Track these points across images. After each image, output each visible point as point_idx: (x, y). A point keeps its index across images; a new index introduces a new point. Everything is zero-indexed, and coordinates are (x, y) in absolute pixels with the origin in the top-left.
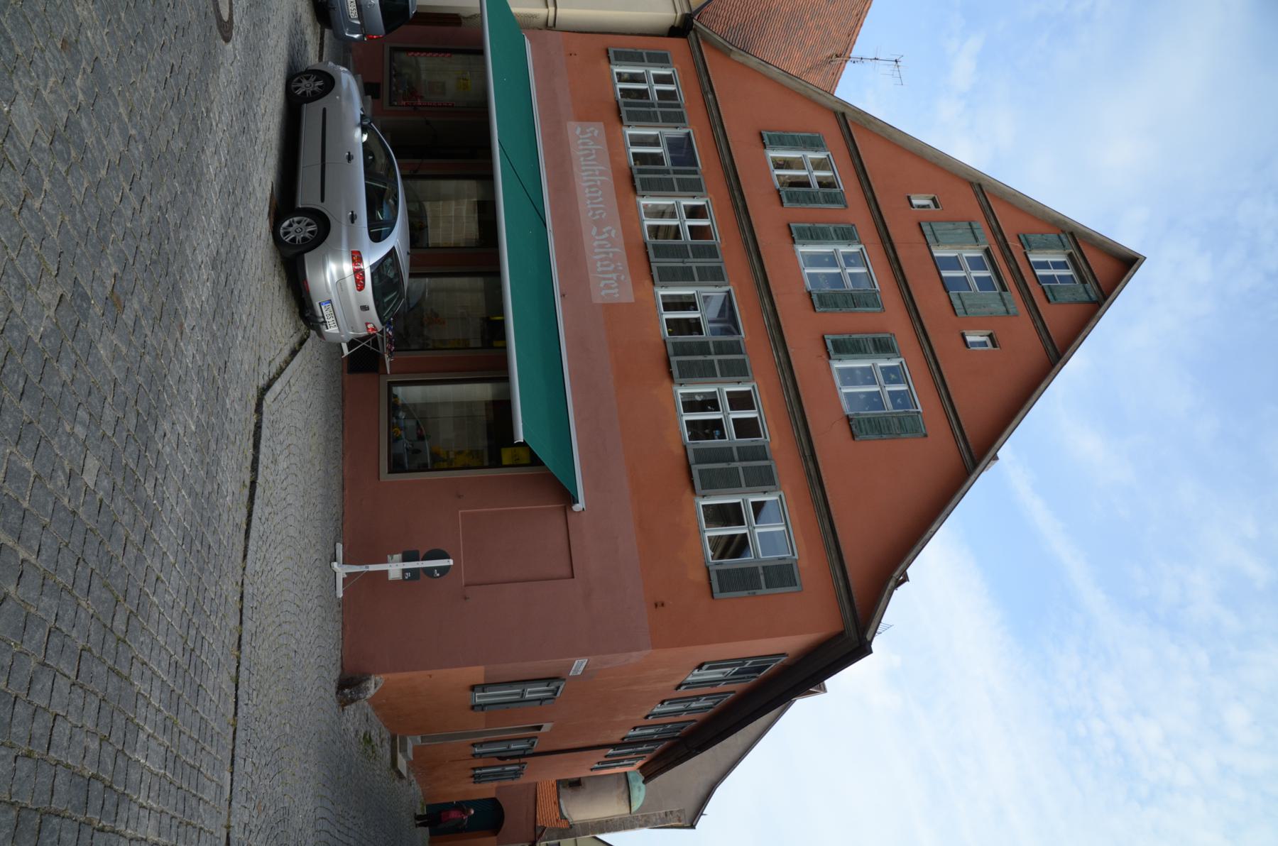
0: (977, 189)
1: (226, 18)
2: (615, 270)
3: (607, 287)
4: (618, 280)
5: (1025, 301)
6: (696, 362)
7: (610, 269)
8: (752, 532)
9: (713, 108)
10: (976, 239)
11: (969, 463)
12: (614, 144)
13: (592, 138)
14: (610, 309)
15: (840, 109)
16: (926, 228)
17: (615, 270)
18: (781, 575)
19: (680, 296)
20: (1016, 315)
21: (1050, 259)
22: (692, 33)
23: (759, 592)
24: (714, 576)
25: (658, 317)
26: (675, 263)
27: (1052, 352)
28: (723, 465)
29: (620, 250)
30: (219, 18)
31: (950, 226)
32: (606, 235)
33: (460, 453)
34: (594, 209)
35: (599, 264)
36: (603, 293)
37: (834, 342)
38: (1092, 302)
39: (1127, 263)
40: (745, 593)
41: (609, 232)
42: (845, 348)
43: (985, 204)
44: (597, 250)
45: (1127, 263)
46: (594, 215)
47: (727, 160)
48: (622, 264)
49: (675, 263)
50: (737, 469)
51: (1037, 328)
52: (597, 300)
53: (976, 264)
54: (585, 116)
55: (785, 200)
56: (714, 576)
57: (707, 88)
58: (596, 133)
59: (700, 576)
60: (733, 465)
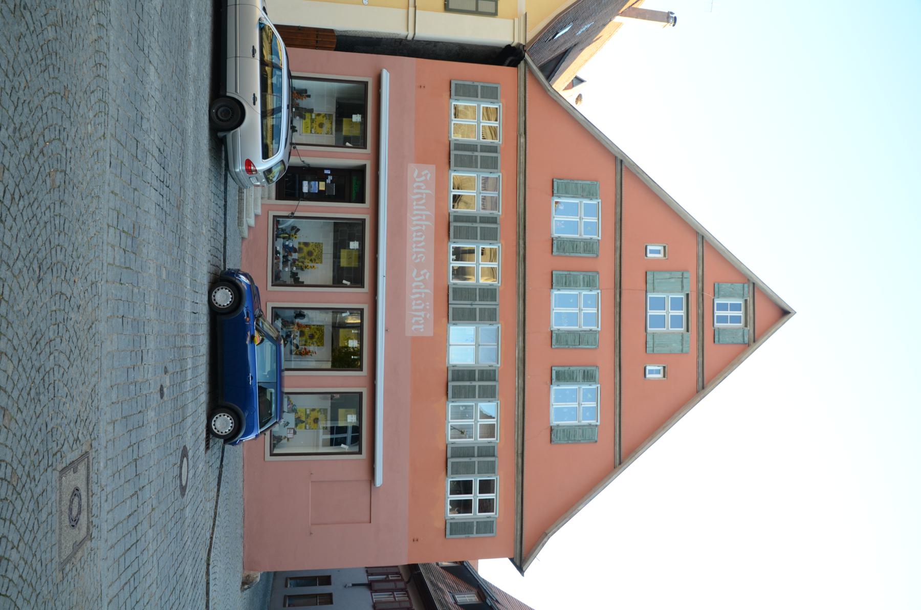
0: (700, 240)
1: (184, 483)
2: (424, 309)
3: (417, 323)
4: (425, 318)
5: (698, 340)
6: (465, 386)
7: (421, 307)
8: (477, 267)
9: (522, 153)
10: (683, 287)
11: (618, 461)
12: (440, 185)
13: (423, 281)
14: (415, 339)
15: (620, 157)
16: (649, 277)
17: (424, 309)
18: (489, 293)
19: (465, 243)
20: (687, 353)
21: (729, 325)
22: (522, 63)
23: (471, 536)
24: (448, 526)
25: (448, 192)
26: (465, 304)
27: (700, 384)
28: (467, 460)
29: (429, 291)
30: (181, 485)
31: (668, 276)
32: (423, 178)
33: (313, 410)
34: (418, 253)
35: (414, 303)
36: (414, 327)
37: (558, 373)
38: (744, 343)
39: (784, 313)
40: (463, 536)
41: (426, 175)
42: (562, 377)
43: (701, 254)
44: (414, 291)
45: (784, 313)
46: (416, 258)
47: (522, 210)
48: (429, 305)
49: (465, 304)
50: (477, 156)
51: (698, 362)
52: (408, 334)
53: (675, 305)
54: (422, 159)
55: (555, 249)
56: (448, 526)
57: (522, 130)
58: (429, 176)
59: (441, 525)
60: (475, 225)
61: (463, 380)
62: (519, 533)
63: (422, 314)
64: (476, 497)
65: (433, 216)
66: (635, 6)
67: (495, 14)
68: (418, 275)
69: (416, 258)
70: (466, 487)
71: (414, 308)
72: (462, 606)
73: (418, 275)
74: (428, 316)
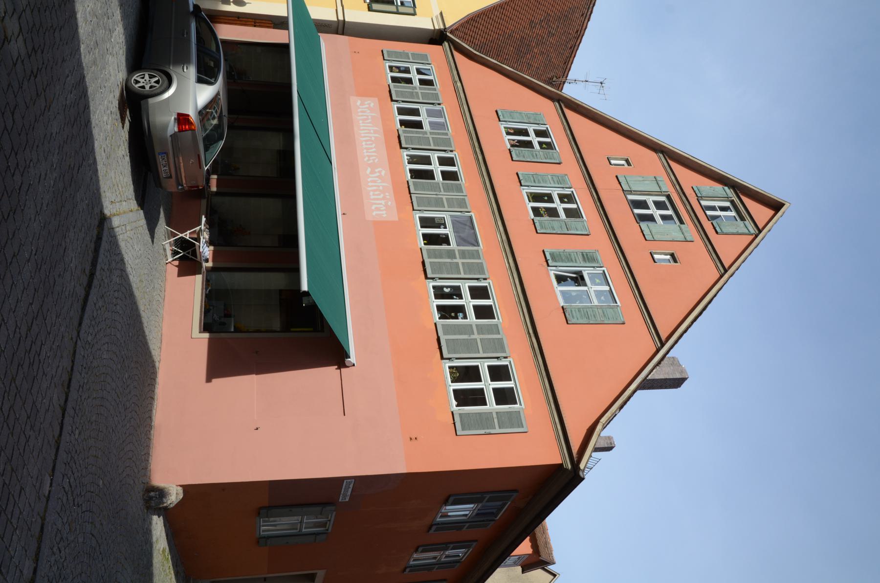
2: (384, 198)
3: (377, 209)
4: (386, 206)
13: (380, 177)
14: (379, 225)
17: (384, 198)
34: (369, 156)
36: (374, 213)
41: (380, 172)
46: (369, 160)
48: (390, 195)
54: (364, 94)
58: (383, 173)
61: (441, 257)
62: (504, 238)
63: (383, 202)
64: (487, 385)
65: (391, 187)
66: (649, 377)
67: (414, 14)
68: (372, 172)
69: (369, 160)
70: (471, 374)
71: (372, 197)
72: (393, 3)
73: (372, 172)
74: (389, 203)
